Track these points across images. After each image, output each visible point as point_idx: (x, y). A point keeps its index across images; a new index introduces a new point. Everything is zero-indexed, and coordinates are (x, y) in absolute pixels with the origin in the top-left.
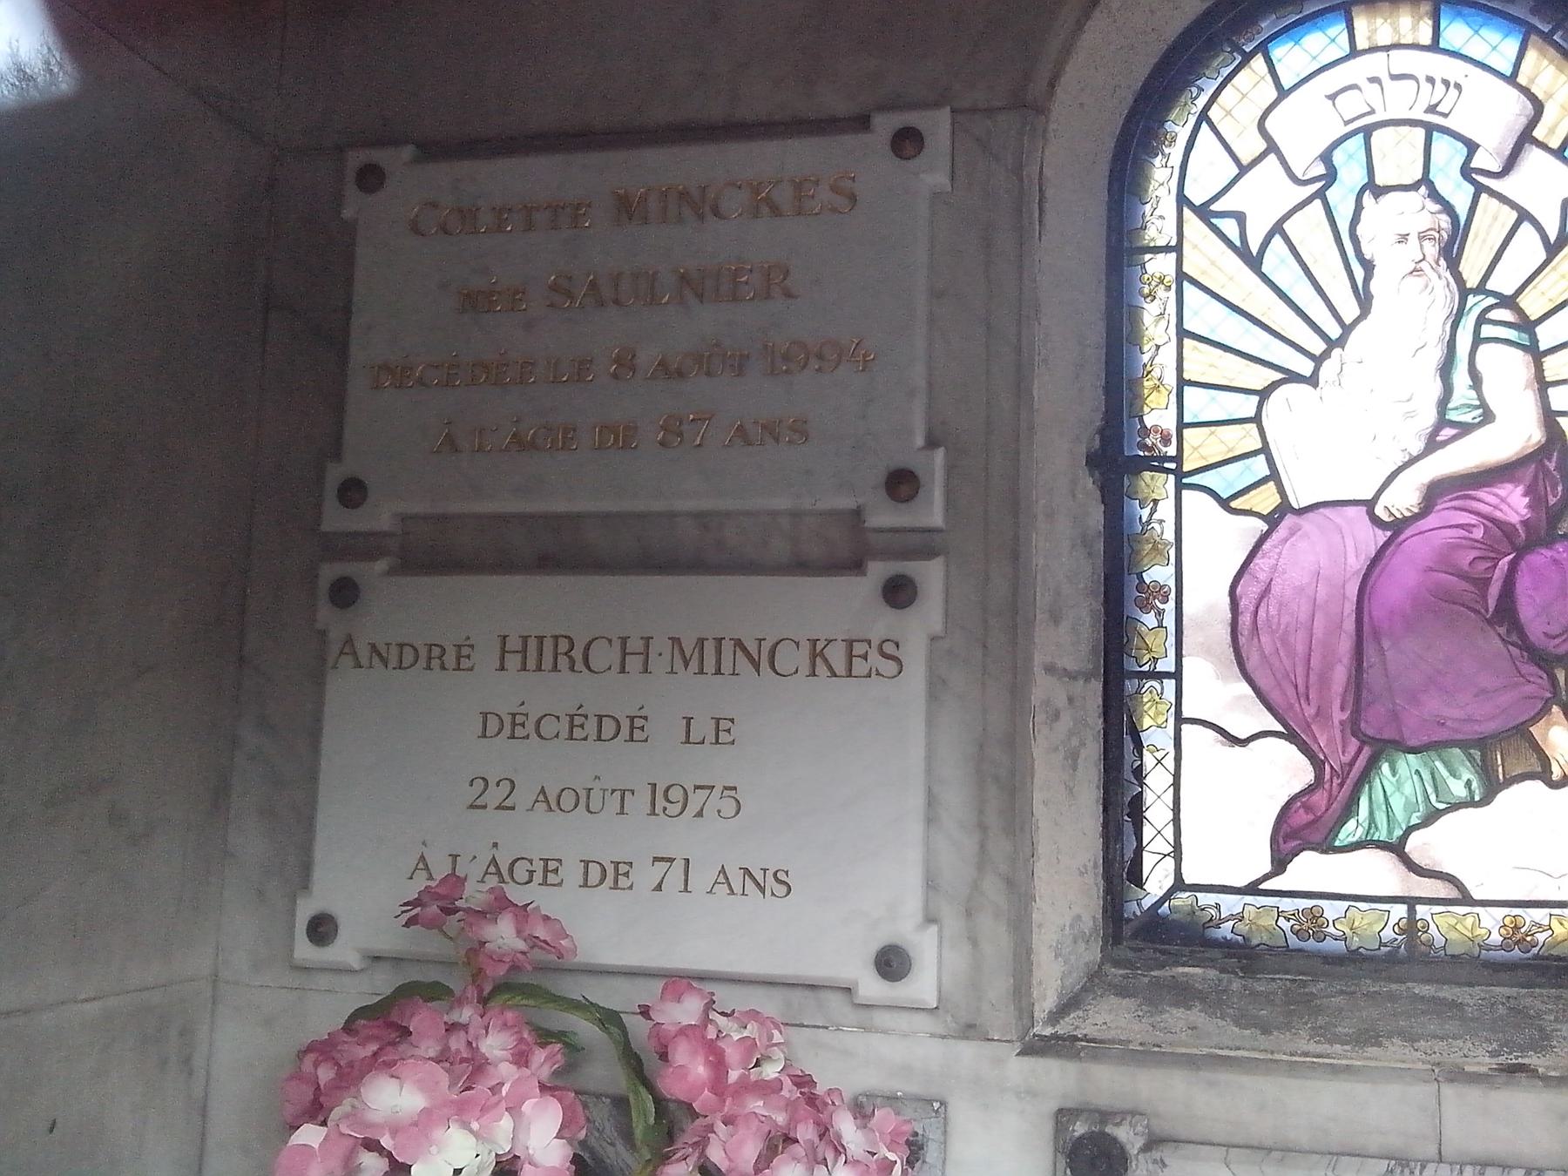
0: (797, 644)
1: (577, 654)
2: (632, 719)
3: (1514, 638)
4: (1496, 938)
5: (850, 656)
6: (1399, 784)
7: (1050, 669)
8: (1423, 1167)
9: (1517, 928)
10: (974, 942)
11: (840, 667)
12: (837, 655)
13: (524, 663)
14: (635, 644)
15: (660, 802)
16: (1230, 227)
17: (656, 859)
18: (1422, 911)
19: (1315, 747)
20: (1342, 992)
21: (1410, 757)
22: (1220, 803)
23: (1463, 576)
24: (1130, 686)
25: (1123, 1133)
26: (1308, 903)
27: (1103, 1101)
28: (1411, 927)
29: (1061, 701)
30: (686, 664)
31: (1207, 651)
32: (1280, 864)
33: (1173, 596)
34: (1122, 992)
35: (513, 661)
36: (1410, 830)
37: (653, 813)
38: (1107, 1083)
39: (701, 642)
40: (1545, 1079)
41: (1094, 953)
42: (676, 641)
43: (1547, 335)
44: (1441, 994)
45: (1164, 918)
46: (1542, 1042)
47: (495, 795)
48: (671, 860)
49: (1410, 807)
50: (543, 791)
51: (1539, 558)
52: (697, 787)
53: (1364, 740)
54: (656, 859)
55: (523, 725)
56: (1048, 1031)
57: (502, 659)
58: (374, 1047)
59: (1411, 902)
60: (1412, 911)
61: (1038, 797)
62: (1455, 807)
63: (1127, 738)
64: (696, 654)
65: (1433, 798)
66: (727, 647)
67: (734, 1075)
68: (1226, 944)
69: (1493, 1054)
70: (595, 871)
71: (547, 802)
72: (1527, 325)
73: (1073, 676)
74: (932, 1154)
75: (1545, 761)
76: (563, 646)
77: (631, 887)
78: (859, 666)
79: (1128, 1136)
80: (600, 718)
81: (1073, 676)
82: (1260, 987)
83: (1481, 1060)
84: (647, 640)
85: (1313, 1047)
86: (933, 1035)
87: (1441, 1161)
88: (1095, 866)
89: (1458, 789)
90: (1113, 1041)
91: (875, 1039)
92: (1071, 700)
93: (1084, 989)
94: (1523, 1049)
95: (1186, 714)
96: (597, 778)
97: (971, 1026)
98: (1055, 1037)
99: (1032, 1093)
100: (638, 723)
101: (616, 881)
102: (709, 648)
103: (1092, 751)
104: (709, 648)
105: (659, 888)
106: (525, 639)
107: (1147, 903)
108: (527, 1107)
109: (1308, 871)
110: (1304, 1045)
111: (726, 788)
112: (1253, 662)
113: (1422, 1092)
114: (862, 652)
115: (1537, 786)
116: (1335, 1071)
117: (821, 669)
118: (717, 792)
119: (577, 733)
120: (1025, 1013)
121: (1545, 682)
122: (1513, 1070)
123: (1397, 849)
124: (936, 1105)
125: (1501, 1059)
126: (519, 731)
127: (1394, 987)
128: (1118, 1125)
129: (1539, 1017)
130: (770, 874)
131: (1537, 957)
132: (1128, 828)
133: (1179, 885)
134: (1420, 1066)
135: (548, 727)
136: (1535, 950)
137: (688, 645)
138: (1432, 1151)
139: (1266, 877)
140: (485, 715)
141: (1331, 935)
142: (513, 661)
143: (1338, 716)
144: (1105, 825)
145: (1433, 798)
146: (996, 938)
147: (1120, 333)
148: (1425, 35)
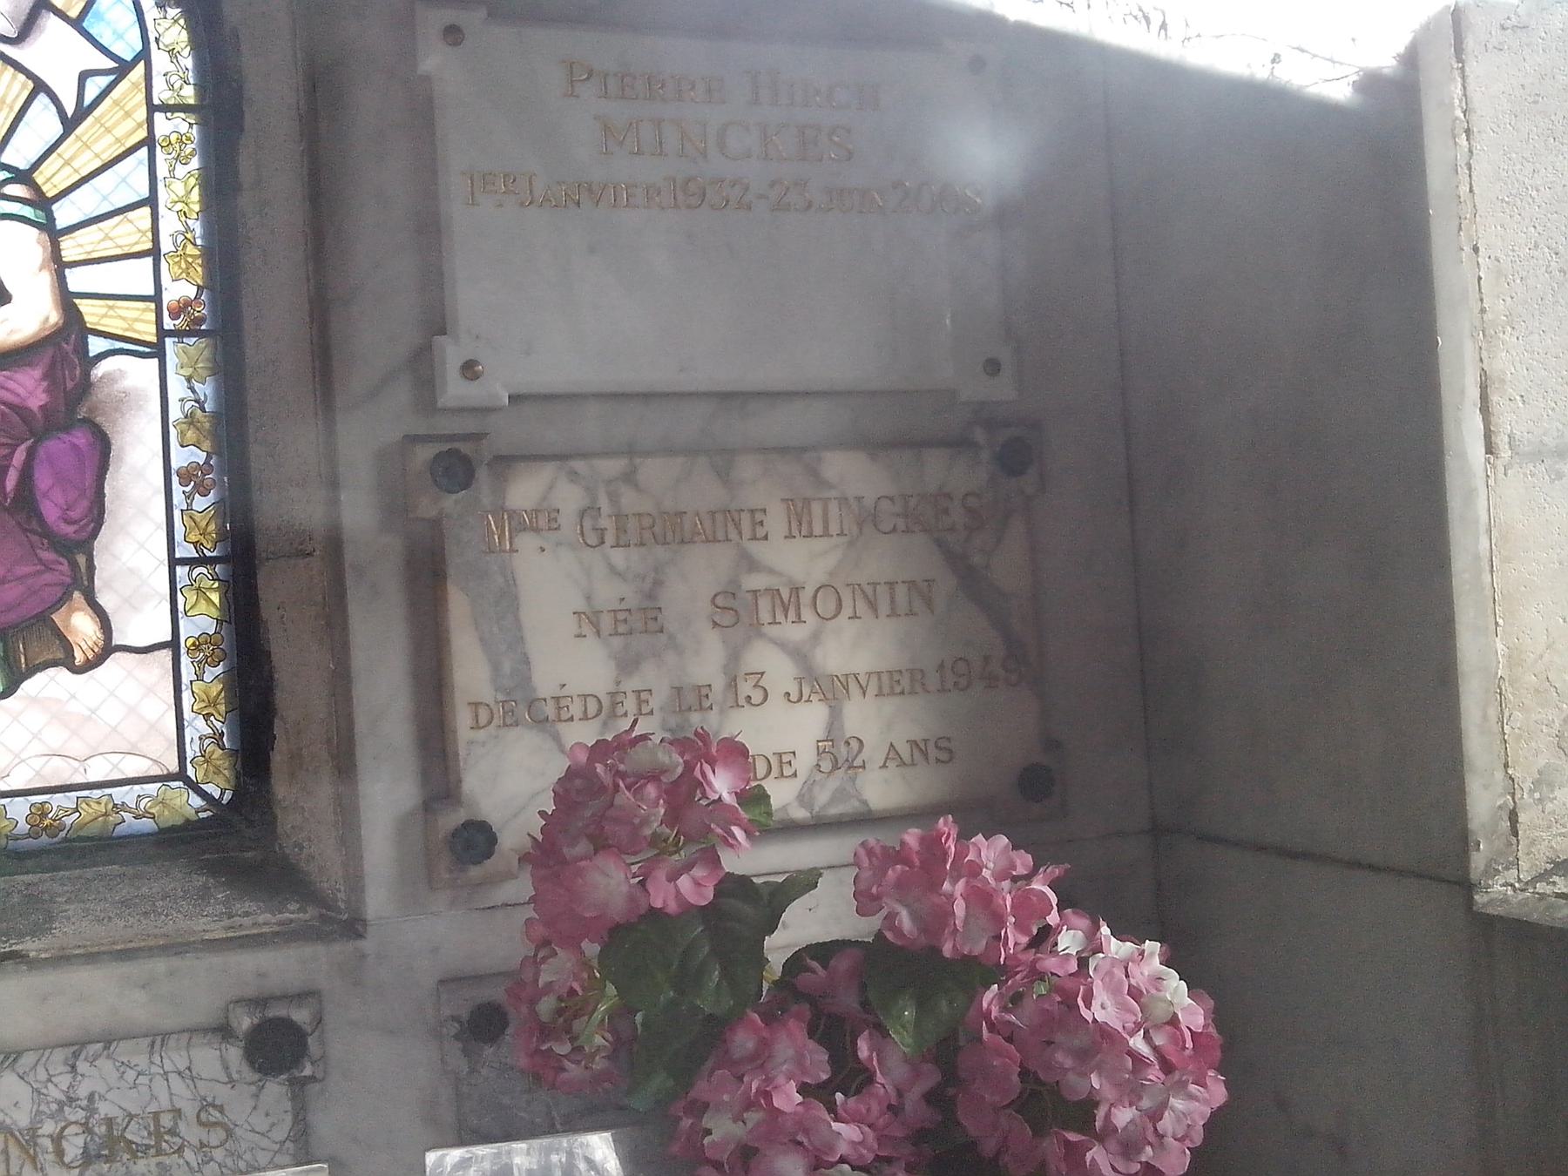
3: (34, 525)
4: (23, 827)
9: (44, 815)
16: (94, 87)
43: (64, 214)
51: (54, 446)
58: (736, 831)
72: (43, 202)
75: (68, 648)
115: (61, 674)
121: (65, 567)
129: (52, 901)
131: (65, 840)
136: (63, 834)
147: (219, 186)
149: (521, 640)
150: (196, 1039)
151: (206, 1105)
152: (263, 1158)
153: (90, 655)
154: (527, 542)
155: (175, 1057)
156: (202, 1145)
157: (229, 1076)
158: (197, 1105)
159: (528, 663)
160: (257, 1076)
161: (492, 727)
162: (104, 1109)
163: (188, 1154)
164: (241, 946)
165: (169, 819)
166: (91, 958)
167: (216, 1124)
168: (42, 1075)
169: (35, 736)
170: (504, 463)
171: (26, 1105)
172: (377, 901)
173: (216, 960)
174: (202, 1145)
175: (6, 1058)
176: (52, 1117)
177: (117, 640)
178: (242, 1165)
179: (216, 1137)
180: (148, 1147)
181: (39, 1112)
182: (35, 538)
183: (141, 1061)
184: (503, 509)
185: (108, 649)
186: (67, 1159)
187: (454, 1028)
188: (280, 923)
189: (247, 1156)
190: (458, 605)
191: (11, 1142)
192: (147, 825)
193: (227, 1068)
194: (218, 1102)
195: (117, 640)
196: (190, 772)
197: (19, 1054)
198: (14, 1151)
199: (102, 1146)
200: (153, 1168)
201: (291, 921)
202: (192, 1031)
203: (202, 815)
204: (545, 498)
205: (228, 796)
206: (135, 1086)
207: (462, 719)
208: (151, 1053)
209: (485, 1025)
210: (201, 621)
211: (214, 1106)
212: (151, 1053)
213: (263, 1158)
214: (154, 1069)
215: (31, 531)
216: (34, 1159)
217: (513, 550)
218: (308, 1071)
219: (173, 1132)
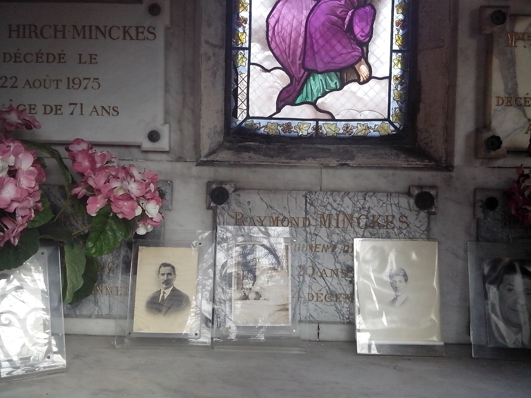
0: (119, 28)
1: (38, 32)
2: (59, 55)
3: (352, 37)
5: (137, 33)
6: (316, 83)
7: (207, 42)
8: (316, 193)
9: (347, 128)
10: (181, 130)
11: (134, 36)
12: (133, 32)
13: (19, 34)
14: (60, 28)
15: (71, 84)
17: (71, 104)
18: (320, 123)
19: (290, 72)
20: (295, 147)
21: (319, 75)
22: (261, 91)
23: (337, 16)
24: (234, 52)
25: (227, 187)
26: (287, 121)
27: (221, 178)
28: (317, 128)
29: (211, 53)
30: (79, 35)
31: (259, 41)
32: (279, 110)
33: (248, 22)
34: (229, 149)
35: (14, 34)
36: (318, 98)
37: (69, 88)
38: (223, 173)
39: (84, 27)
40: (352, 167)
41: (221, 139)
42: (75, 27)
44: (324, 147)
45: (243, 128)
46: (352, 158)
47: (9, 83)
48: (76, 104)
49: (318, 91)
50: (28, 81)
51: (361, 11)
52: (85, 79)
53: (306, 69)
54: (71, 104)
55: (19, 57)
56: (205, 159)
57: (10, 34)
59: (317, 120)
60: (317, 123)
61: (202, 85)
62: (332, 90)
63: (233, 70)
64: (82, 31)
65: (325, 87)
66: (94, 29)
67: (98, 165)
68: (263, 136)
69: (338, 161)
70: (48, 109)
71: (29, 84)
73: (215, 46)
74: (168, 197)
75: (359, 76)
76: (33, 28)
77: (62, 114)
78: (141, 36)
79: (229, 188)
80: (48, 54)
81: (215, 46)
82: (271, 147)
83: (334, 162)
84: (64, 26)
85: (286, 161)
86: (168, 161)
87: (321, 191)
88: (222, 111)
89: (333, 85)
90: (225, 162)
91: (149, 163)
92: (214, 54)
93: (217, 149)
94: (347, 160)
95: (252, 62)
96: (48, 76)
97: (180, 158)
98: (207, 161)
99: (199, 177)
100: (62, 56)
101: (56, 112)
102: (87, 29)
103: (221, 73)
104: (87, 29)
105: (72, 114)
106: (18, 26)
107: (238, 123)
108: (20, 156)
109: (288, 111)
110: (283, 161)
111: (95, 79)
112: (273, 45)
113: (316, 172)
114: (142, 31)
116: (291, 167)
117: (127, 37)
118: (92, 80)
119: (40, 60)
120: (197, 146)
122: (342, 165)
123: (314, 104)
124: (169, 182)
125: (340, 162)
126: (18, 59)
127: (311, 145)
128: (226, 185)
130: (111, 108)
132: (233, 99)
133: (248, 117)
134: (316, 165)
135: (28, 58)
137: (79, 28)
138: (319, 188)
139: (274, 114)
140: (5, 54)
141: (293, 131)
142: (14, 34)
143: (298, 62)
144: (225, 98)
145: (325, 87)
146: (188, 129)
148: (396, 47)
149: (515, 77)
150: (400, 195)
151: (402, 216)
152: (418, 235)
153: (365, 79)
154: (520, 44)
155: (394, 199)
156: (400, 228)
157: (410, 208)
158: (400, 215)
159: (517, 85)
160: (418, 209)
161: (503, 106)
162: (372, 212)
163: (395, 230)
164: (416, 170)
165: (383, 133)
166: (369, 167)
167: (404, 222)
168: (356, 200)
169: (372, 88)
170: (516, 17)
171: (351, 207)
172: (458, 160)
173: (406, 172)
174: (400, 228)
175: (345, 193)
176: (357, 212)
177: (373, 75)
178: (411, 236)
179: (404, 226)
180: (384, 226)
181: (354, 210)
182: (352, 41)
183: (385, 199)
184: (513, 32)
185: (371, 77)
186: (360, 226)
187: (480, 204)
188: (424, 165)
189: (413, 234)
190: (496, 63)
191: (345, 217)
192: (377, 134)
193: (409, 205)
194: (406, 215)
195: (373, 75)
196: (391, 119)
197: (349, 193)
198: (346, 220)
199: (371, 223)
200: (385, 232)
201: (427, 165)
202: (399, 193)
203: (393, 133)
204: (527, 29)
205: (402, 127)
206: (382, 206)
207: (494, 102)
208: (388, 197)
209: (490, 204)
210: (397, 71)
211: (404, 216)
212: (388, 197)
213: (418, 235)
214: (388, 202)
215: (352, 39)
216: (351, 224)
217: (515, 46)
218: (433, 210)
219: (391, 222)
